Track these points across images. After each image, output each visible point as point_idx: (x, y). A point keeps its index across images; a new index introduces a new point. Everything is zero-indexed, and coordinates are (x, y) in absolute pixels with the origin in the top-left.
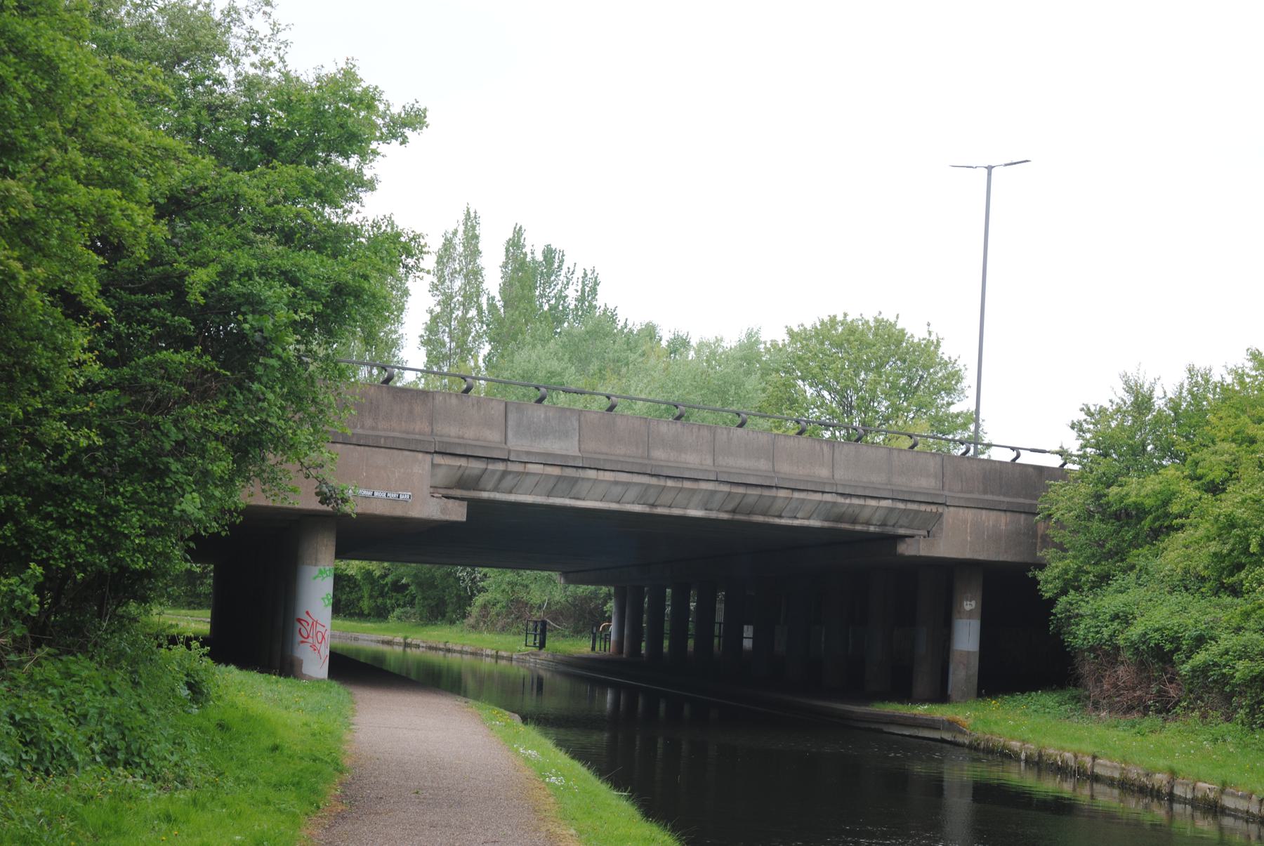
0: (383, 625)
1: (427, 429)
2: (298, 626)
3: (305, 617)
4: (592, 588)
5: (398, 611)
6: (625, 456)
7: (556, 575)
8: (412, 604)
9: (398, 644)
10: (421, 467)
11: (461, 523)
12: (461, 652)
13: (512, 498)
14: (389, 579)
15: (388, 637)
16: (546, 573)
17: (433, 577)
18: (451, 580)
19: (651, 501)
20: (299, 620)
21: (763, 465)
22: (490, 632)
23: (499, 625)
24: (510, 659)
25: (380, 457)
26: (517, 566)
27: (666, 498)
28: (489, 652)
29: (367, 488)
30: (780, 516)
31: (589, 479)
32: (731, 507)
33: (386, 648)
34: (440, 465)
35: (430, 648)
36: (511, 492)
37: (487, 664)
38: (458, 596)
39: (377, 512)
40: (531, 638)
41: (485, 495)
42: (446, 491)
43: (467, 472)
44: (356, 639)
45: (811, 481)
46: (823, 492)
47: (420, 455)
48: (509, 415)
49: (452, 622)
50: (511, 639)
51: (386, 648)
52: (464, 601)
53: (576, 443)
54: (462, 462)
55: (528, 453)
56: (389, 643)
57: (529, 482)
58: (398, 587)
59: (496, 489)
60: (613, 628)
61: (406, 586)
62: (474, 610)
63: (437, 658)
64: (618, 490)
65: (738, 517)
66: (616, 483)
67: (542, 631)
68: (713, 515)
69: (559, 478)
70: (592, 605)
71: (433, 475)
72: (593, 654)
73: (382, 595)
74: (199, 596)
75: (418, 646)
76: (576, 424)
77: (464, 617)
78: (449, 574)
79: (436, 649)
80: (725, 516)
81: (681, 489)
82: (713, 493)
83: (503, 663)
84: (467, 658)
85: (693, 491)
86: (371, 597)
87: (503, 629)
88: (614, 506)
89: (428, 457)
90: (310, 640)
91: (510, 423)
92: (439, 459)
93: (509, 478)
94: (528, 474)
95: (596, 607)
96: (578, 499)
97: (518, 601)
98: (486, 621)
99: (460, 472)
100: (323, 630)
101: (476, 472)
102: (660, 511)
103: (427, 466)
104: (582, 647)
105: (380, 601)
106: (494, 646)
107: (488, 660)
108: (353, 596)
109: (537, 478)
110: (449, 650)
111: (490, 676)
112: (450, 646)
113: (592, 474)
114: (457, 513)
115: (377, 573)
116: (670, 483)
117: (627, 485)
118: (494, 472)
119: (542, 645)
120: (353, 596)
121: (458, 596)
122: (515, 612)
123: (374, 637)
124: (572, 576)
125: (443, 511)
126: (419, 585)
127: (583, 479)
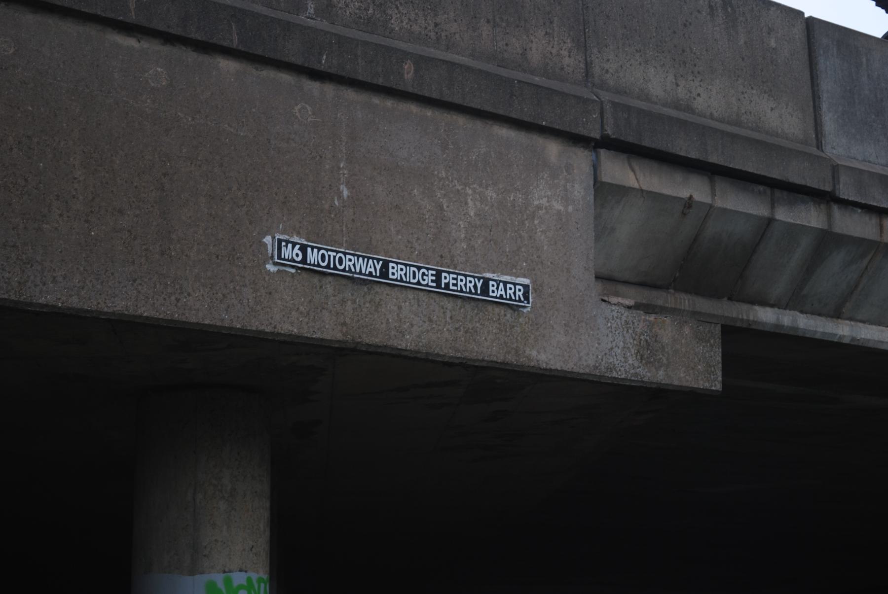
10: (558, 188)
13: (843, 330)
29: (365, 249)
36: (837, 314)
39: (407, 342)
41: (766, 316)
42: (689, 270)
45: (791, 333)
47: (553, 149)
54: (695, 189)
59: (795, 300)
89: (581, 159)
91: (827, 86)
92: (618, 171)
103: (580, 190)
114: (691, 362)
118: (793, 231)
125: (648, 350)
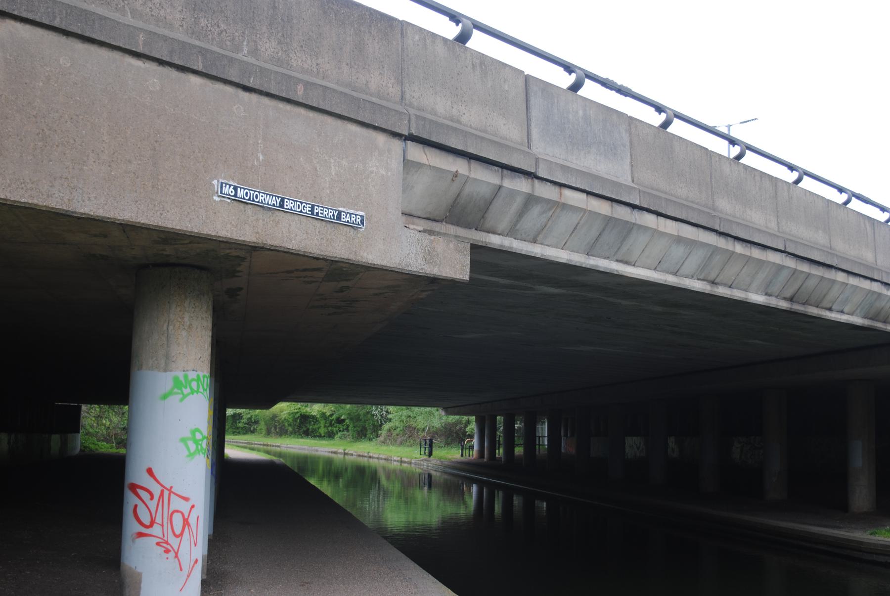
0: (332, 442)
1: (393, 91)
2: (130, 499)
3: (144, 480)
4: (457, 417)
5: (340, 434)
6: (299, 449)
7: (433, 410)
8: (347, 430)
9: (341, 453)
10: (384, 159)
11: (453, 284)
12: (378, 458)
14: (334, 417)
15: (334, 449)
16: (428, 409)
17: (359, 415)
18: (369, 416)
19: (712, 276)
20: (134, 488)
21: (820, 238)
22: (393, 445)
23: (398, 441)
24: (411, 463)
25: (298, 125)
26: (408, 404)
27: (731, 272)
28: (395, 458)
30: (830, 309)
31: (646, 229)
32: (789, 293)
33: (334, 456)
34: (419, 165)
35: (359, 456)
36: (534, 241)
37: (395, 465)
38: (374, 425)
40: (423, 449)
41: (495, 241)
43: (468, 189)
44: (317, 451)
46: (872, 280)
47: (381, 139)
48: (533, 101)
49: (370, 440)
50: (408, 449)
51: (334, 456)
52: (377, 428)
53: (627, 167)
54: (460, 166)
55: (565, 169)
56: (335, 453)
57: (566, 221)
58: (340, 421)
59: (512, 232)
60: (475, 441)
61: (343, 420)
62: (383, 432)
63: (364, 461)
64: (678, 252)
65: (797, 307)
66: (679, 240)
67: (429, 446)
68: (774, 302)
69: (609, 220)
70: (458, 428)
71: (406, 188)
72: (463, 459)
73: (331, 425)
74: (238, 428)
75: (352, 455)
76: (626, 137)
77: (377, 436)
78: (368, 413)
79: (363, 456)
80: (784, 305)
81: (749, 259)
82: (781, 268)
83: (405, 465)
84: (382, 462)
85: (761, 263)
86: (325, 426)
87: (401, 444)
88: (671, 280)
89: (397, 145)
90: (156, 530)
91: (535, 113)
92: (416, 153)
93: (536, 210)
94: (564, 206)
95: (460, 429)
96: (627, 263)
97: (409, 427)
98: (391, 438)
99: (455, 188)
100: (184, 507)
101: (485, 192)
102: (722, 291)
103: (396, 164)
104: (454, 454)
105: (330, 428)
106: (399, 454)
107: (395, 463)
108: (316, 426)
109: (574, 218)
110: (370, 457)
111: (394, 471)
112: (371, 455)
113: (649, 220)
114: (454, 265)
115: (328, 414)
116: (739, 248)
117: (692, 244)
118: (513, 193)
119: (430, 454)
120: (316, 426)
121: (374, 425)
122: (409, 433)
123: (327, 449)
124: (448, 411)
125: (429, 256)
126: (351, 419)
127: (640, 227)
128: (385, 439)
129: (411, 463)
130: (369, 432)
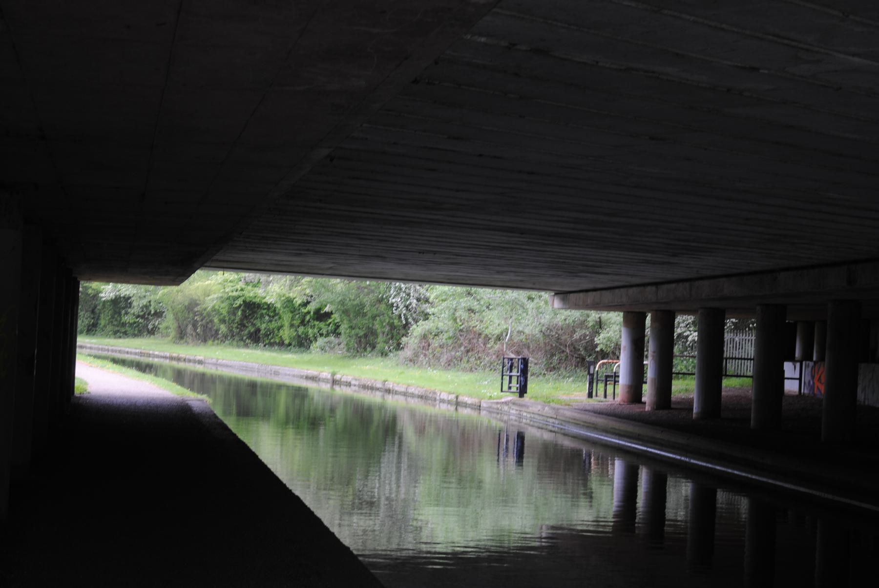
24: (478, 408)
35: (365, 387)
49: (384, 354)
62: (411, 341)
75: (349, 384)
79: (372, 388)
110: (388, 391)
119: (522, 391)
121: (392, 326)
128: (416, 355)
129: (478, 408)
130: (381, 339)
